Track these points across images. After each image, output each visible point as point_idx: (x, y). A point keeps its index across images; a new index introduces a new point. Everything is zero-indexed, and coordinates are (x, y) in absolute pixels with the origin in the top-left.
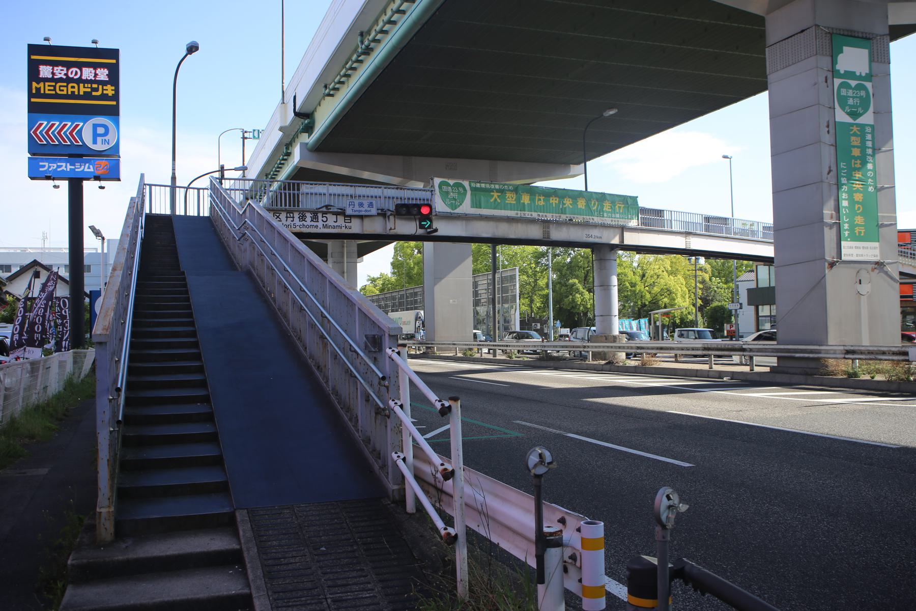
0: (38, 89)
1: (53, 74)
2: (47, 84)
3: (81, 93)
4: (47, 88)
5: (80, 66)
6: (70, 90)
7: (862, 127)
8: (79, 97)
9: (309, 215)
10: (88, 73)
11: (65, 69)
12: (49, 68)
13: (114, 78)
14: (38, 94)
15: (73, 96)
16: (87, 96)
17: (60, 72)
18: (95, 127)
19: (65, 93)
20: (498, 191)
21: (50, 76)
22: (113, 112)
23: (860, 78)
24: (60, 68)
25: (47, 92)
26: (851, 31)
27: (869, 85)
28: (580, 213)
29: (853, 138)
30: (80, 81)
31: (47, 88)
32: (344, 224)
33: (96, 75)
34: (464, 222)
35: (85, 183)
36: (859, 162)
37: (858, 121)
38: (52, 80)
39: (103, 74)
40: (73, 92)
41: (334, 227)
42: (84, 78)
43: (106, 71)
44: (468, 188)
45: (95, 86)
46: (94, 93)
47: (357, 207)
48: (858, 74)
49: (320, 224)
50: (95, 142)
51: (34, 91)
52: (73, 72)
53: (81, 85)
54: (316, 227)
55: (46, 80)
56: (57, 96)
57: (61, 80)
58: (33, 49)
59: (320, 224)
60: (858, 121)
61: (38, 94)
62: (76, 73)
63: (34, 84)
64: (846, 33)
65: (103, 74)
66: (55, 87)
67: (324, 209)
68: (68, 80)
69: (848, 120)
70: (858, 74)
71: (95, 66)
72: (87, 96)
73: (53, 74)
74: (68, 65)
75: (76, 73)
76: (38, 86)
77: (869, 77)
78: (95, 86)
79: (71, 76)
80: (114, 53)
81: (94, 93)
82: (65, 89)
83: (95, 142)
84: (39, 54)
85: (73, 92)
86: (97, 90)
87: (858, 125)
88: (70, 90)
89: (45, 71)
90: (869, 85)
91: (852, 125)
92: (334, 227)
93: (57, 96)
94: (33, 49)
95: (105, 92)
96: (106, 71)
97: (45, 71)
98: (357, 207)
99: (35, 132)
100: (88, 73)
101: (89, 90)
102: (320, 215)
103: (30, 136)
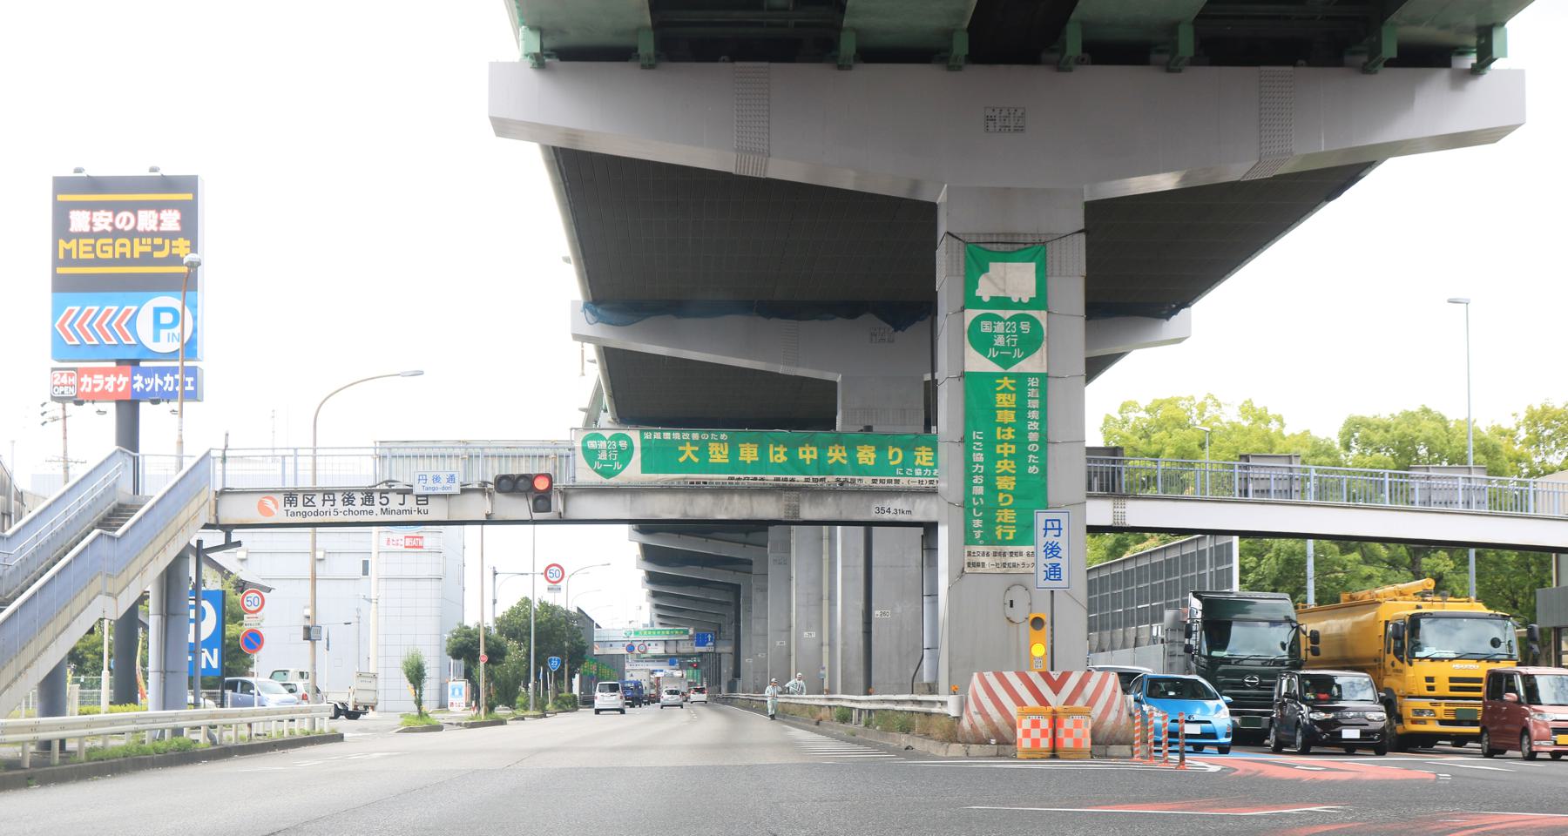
0: (68, 252)
1: (91, 224)
2: (82, 241)
3: (136, 255)
4: (82, 250)
5: (134, 207)
6: (118, 250)
7: (1021, 378)
8: (132, 262)
9: (358, 497)
10: (147, 220)
11: (110, 214)
12: (85, 215)
13: (189, 229)
14: (68, 260)
15: (123, 261)
16: (146, 259)
17: (102, 220)
18: (157, 311)
19: (109, 256)
20: (693, 443)
21: (86, 229)
22: (186, 283)
23: (1020, 305)
24: (103, 213)
25: (82, 256)
26: (1013, 235)
27: (1040, 316)
28: (864, 470)
29: (999, 396)
30: (133, 234)
31: (82, 249)
32: (415, 507)
33: (160, 222)
34: (628, 497)
35: (142, 405)
36: (1009, 430)
37: (1013, 369)
38: (91, 234)
39: (171, 220)
40: (123, 255)
41: (400, 512)
42: (140, 228)
43: (176, 215)
44: (637, 444)
45: (158, 241)
46: (157, 255)
47: (430, 484)
48: (1015, 300)
49: (377, 508)
50: (157, 338)
51: (61, 256)
52: (124, 220)
53: (136, 241)
54: (371, 512)
55: (81, 235)
56: (98, 262)
57: (104, 234)
58: (61, 185)
59: (377, 508)
60: (1013, 369)
61: (68, 260)
62: (128, 221)
63: (62, 242)
64: (1002, 239)
65: (171, 220)
66: (94, 246)
67: (384, 487)
68: (116, 234)
69: (994, 368)
70: (1015, 300)
71: (159, 207)
72: (146, 259)
73: (91, 224)
74: (116, 208)
75: (128, 221)
76: (68, 247)
77: (1035, 303)
78: (158, 241)
79: (119, 226)
80: (188, 184)
81: (157, 255)
82: (110, 249)
83: (157, 338)
84: (76, 190)
85: (123, 255)
86: (161, 248)
87: (1010, 376)
88: (118, 250)
89: (79, 221)
90: (1040, 316)
91: (1001, 376)
92: (400, 512)
93: (98, 262)
94: (61, 185)
95: (174, 251)
96: (176, 215)
97: (79, 221)
98: (430, 484)
99: (61, 326)
100: (147, 220)
101: (148, 249)
102: (376, 496)
103: (54, 329)
